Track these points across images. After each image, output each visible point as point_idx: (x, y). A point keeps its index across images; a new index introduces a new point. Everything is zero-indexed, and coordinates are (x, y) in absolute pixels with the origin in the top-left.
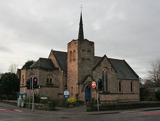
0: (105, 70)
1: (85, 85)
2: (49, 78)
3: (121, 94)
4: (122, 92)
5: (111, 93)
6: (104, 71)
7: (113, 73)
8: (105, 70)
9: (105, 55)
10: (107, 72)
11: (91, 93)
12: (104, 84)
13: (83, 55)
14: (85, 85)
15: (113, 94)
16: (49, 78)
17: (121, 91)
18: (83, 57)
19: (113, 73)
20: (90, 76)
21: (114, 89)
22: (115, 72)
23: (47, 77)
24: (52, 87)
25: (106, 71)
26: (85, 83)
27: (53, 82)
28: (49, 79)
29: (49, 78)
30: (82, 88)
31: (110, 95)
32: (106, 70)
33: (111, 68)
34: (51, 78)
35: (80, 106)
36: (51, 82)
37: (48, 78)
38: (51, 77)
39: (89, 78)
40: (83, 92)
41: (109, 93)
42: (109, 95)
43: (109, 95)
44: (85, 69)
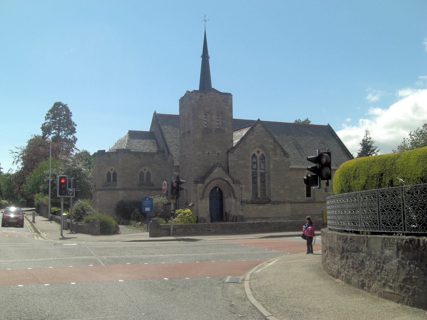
0: (258, 152)
1: (207, 185)
2: (145, 173)
3: (310, 202)
4: (314, 198)
5: (241, 199)
6: (257, 155)
7: (277, 159)
8: (258, 152)
9: (328, 124)
10: (265, 155)
11: (224, 201)
12: (51, 193)
13: (206, 123)
14: (207, 185)
15: (278, 203)
16: (145, 173)
17: (312, 195)
18: (206, 126)
19: (277, 159)
20: (221, 166)
21: (282, 192)
22: (284, 156)
23: (141, 170)
24: (151, 190)
25: (263, 154)
26: (207, 181)
27: (152, 180)
28: (143, 173)
29: (143, 171)
30: (201, 191)
31: (270, 205)
32: (261, 153)
33: (272, 146)
34: (148, 172)
35: (113, 240)
36: (150, 181)
37: (142, 172)
38: (148, 169)
39: (216, 171)
40: (203, 200)
41: (268, 201)
42: (267, 206)
43: (268, 204)
44: (211, 152)
